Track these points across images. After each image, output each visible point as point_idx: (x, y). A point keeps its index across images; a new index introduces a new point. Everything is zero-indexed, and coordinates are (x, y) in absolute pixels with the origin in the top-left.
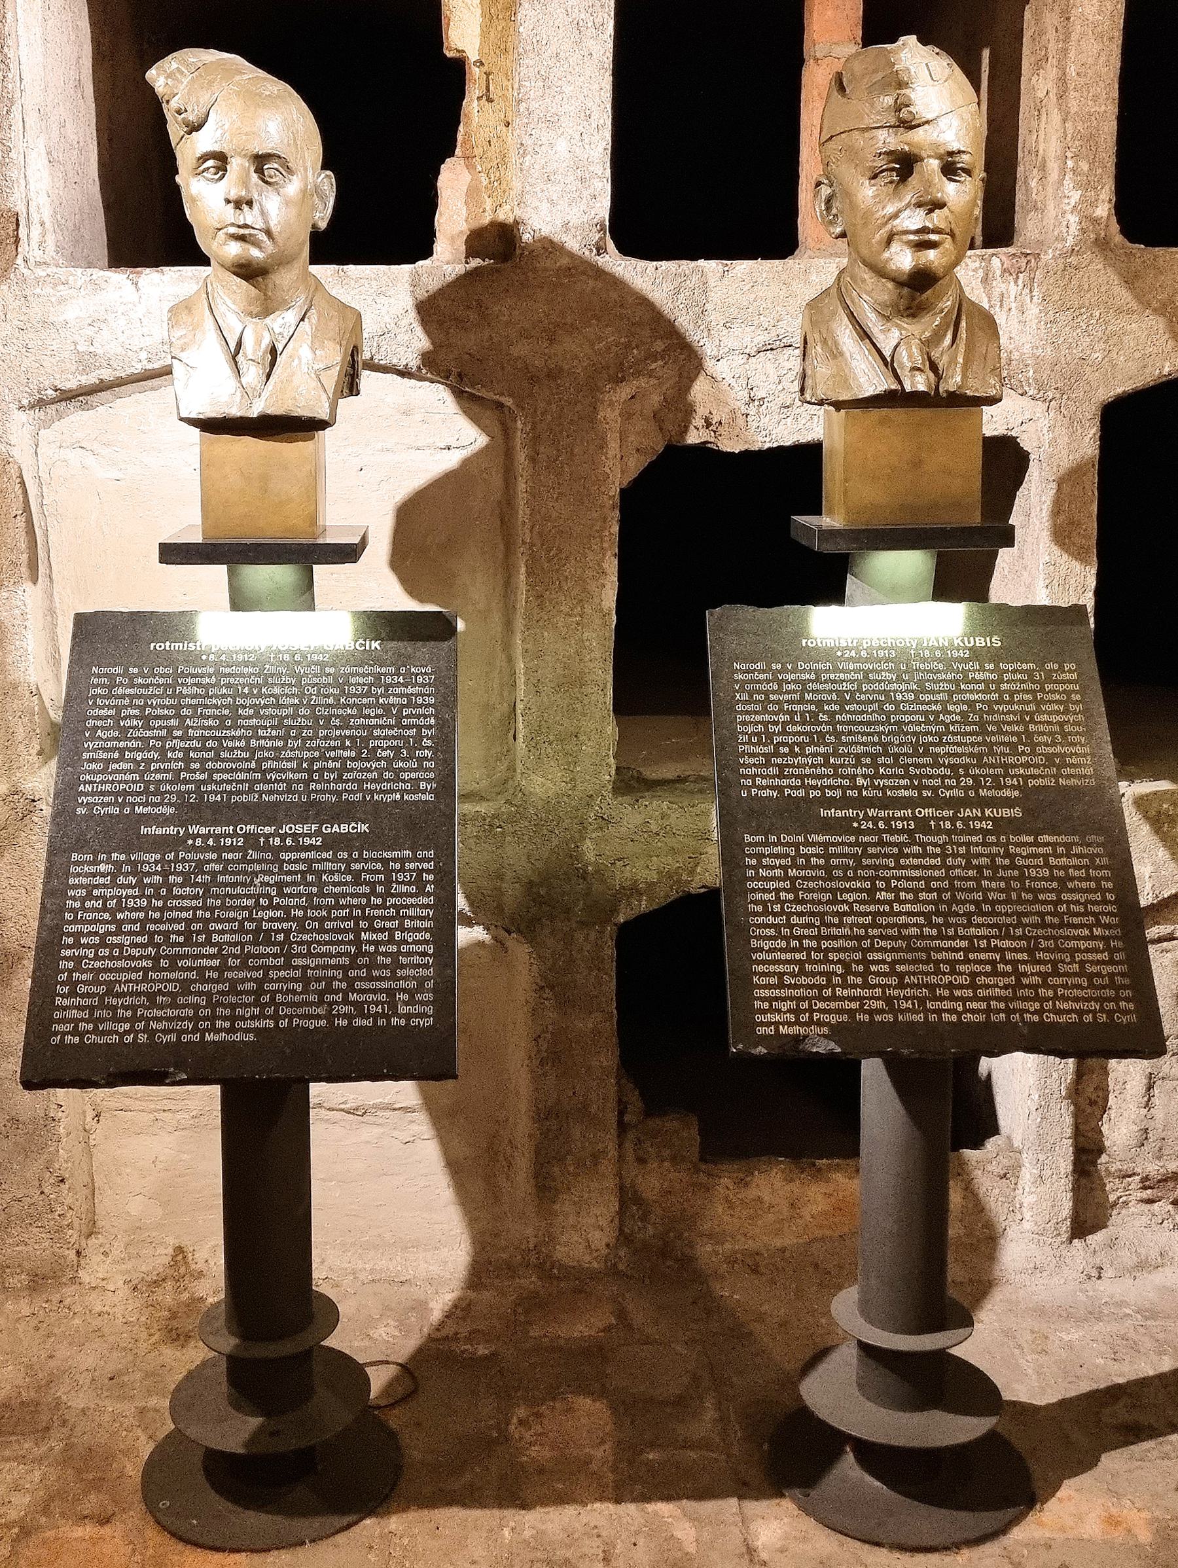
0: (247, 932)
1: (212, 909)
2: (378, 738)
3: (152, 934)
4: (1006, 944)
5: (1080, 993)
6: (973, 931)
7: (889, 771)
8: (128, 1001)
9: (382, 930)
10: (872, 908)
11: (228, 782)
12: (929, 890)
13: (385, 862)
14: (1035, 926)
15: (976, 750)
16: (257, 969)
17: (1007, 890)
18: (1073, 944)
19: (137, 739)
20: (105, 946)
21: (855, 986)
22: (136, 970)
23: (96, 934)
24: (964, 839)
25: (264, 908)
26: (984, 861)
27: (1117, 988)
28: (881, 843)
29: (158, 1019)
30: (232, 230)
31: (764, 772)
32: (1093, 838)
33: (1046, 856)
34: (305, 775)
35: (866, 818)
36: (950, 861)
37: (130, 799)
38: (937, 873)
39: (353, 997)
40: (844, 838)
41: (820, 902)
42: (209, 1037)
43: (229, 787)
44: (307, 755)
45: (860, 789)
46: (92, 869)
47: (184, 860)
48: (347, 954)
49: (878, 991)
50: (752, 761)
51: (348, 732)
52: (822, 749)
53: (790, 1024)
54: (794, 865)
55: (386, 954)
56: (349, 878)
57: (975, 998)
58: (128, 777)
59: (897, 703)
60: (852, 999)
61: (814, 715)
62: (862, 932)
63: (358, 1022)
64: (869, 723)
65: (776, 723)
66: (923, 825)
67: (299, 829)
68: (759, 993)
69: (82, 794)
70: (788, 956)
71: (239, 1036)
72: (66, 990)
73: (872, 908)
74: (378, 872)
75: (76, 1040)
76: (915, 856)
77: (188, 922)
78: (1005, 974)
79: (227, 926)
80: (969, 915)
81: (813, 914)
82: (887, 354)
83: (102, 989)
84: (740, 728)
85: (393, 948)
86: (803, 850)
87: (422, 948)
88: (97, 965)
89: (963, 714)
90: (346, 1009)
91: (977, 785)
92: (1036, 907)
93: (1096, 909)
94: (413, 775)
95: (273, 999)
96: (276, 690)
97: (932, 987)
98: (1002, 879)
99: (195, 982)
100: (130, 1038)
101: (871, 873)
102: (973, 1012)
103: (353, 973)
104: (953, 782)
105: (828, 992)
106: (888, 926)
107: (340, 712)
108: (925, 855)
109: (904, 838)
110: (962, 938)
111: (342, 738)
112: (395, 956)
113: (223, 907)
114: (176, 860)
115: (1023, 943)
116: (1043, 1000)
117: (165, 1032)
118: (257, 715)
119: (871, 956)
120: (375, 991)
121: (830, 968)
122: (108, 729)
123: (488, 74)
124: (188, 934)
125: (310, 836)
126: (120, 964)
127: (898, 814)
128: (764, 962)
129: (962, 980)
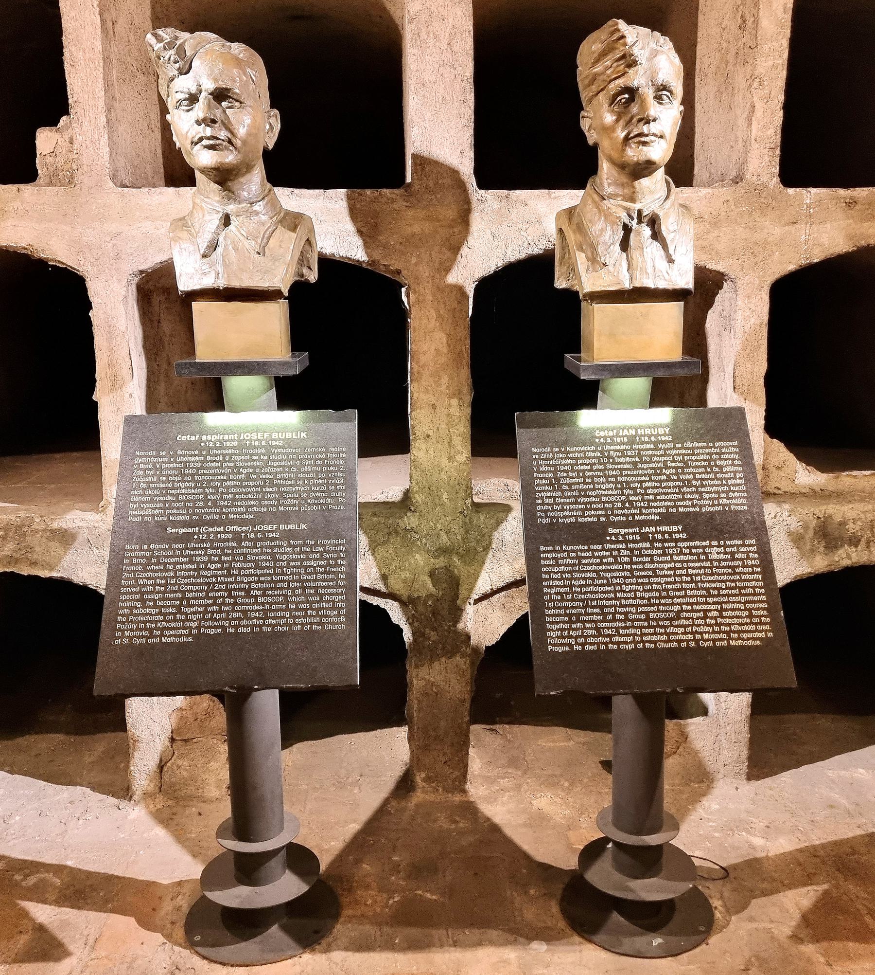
30: (205, 142)
67: (265, 527)
125: (272, 532)
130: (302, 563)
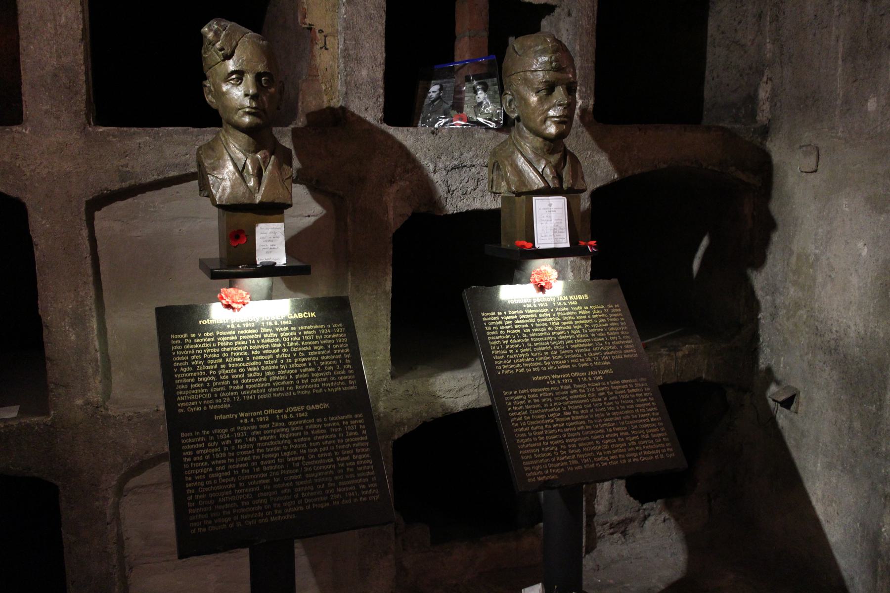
0: (280, 464)
1: (260, 454)
2: (324, 360)
3: (232, 470)
4: (619, 429)
5: (652, 447)
6: (605, 425)
7: (557, 358)
8: (227, 506)
9: (346, 455)
10: (563, 419)
11: (255, 389)
12: (584, 409)
13: (340, 421)
14: (628, 420)
15: (589, 345)
16: (289, 481)
17: (615, 405)
18: (644, 426)
19: (203, 371)
20: (209, 479)
21: (564, 455)
22: (227, 490)
23: (203, 474)
24: (593, 385)
25: (286, 451)
26: (603, 394)
27: (665, 443)
28: (560, 390)
29: (245, 514)
31: (505, 362)
32: (642, 379)
33: (626, 389)
34: (292, 382)
35: (552, 379)
36: (589, 395)
37: (206, 402)
38: (585, 401)
39: (339, 490)
40: (545, 389)
41: (541, 419)
42: (273, 519)
43: (255, 392)
44: (290, 372)
45: (546, 366)
46: (193, 440)
47: (240, 431)
48: (332, 469)
49: (574, 456)
50: (499, 357)
51: (309, 359)
52: (527, 350)
53: (542, 476)
54: (527, 404)
55: (350, 467)
56: (324, 431)
57: (612, 454)
58: (202, 391)
59: (553, 327)
60: (564, 461)
61: (520, 334)
62: (561, 431)
63: (344, 502)
64: (544, 336)
65: (505, 339)
66: (575, 379)
67: (295, 409)
68: (525, 463)
69: (180, 402)
70: (534, 445)
71: (288, 517)
72: (193, 504)
73: (563, 419)
74: (337, 427)
75: (204, 530)
76: (575, 394)
77: (249, 462)
78: (622, 442)
79: (270, 462)
80: (602, 418)
81: (539, 425)
82: (540, 170)
83: (212, 502)
84: (491, 343)
85: (353, 464)
86: (530, 396)
87: (367, 462)
88: (207, 489)
89: (580, 329)
90: (337, 496)
91: (593, 361)
92: (627, 412)
93: (650, 410)
94: (344, 378)
95: (300, 495)
96: (269, 341)
97: (595, 452)
98: (317, 441)
99: (259, 492)
100: (232, 525)
101: (559, 404)
102: (613, 460)
103: (336, 478)
104: (583, 360)
105: (553, 459)
106: (572, 426)
107: (303, 349)
108: (579, 393)
109: (569, 387)
110: (602, 428)
111: (307, 362)
112: (355, 467)
113: (265, 453)
114: (236, 431)
115: (625, 428)
116: (638, 451)
117: (250, 519)
118: (261, 354)
119: (568, 441)
120: (349, 486)
121: (552, 448)
122: (186, 366)
123: (325, 36)
124: (250, 468)
125: (301, 412)
126: (219, 488)
127: (564, 376)
128: (524, 449)
129: (606, 447)
130: (262, 433)
